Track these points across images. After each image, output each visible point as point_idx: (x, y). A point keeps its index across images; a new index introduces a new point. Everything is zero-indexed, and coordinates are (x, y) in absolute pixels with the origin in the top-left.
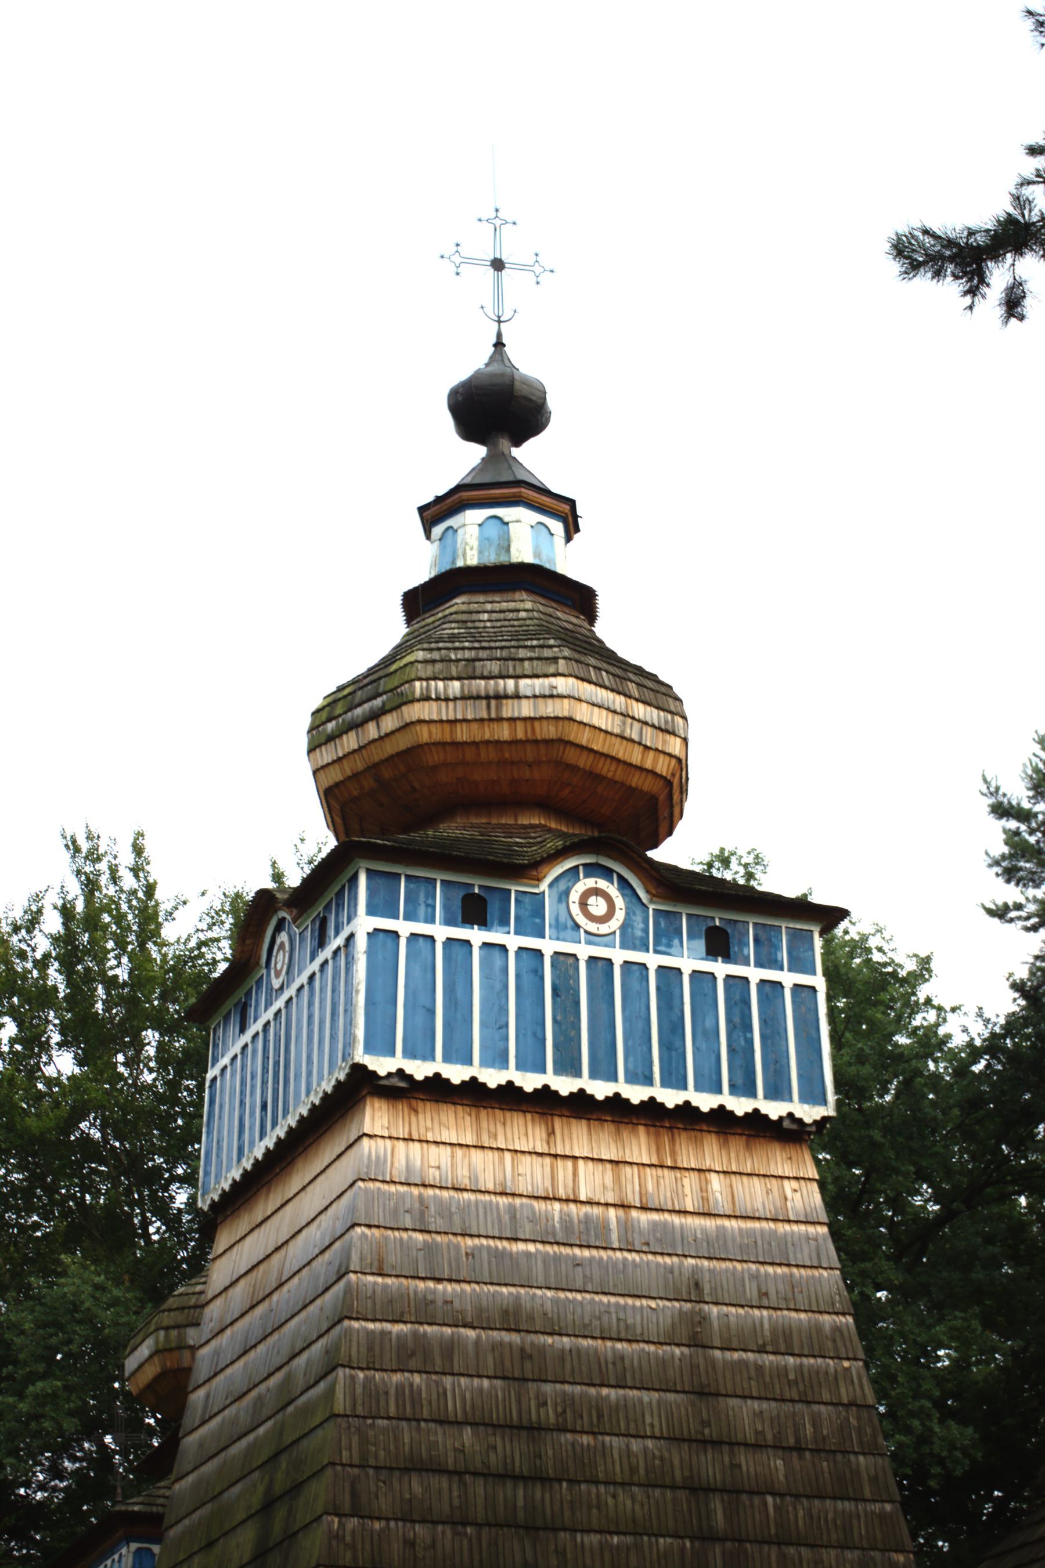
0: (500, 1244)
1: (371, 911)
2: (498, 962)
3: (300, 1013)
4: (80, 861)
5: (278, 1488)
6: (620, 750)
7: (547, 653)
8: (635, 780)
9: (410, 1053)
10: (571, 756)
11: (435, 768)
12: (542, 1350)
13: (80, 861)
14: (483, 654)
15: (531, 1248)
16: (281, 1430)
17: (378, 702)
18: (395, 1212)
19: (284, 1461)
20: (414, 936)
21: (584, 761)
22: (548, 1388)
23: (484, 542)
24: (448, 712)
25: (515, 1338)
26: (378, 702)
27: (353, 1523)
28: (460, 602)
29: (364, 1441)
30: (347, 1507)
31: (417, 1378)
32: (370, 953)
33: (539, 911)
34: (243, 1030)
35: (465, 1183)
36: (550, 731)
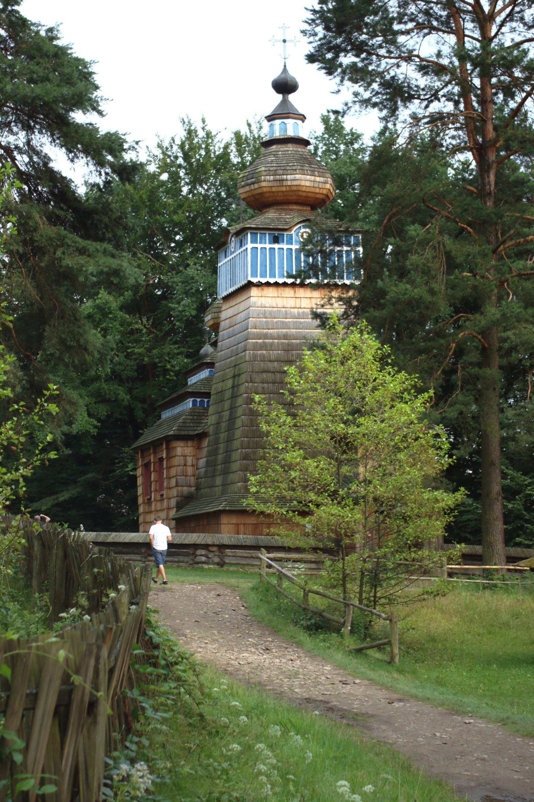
0: (283, 320)
1: (252, 242)
2: (282, 252)
3: (237, 259)
4: (185, 126)
5: (236, 374)
6: (313, 190)
7: (294, 168)
8: (318, 196)
9: (261, 276)
10: (301, 193)
11: (268, 197)
12: (293, 343)
13: (185, 126)
14: (279, 168)
15: (290, 320)
16: (236, 360)
17: (253, 180)
18: (258, 314)
19: (237, 367)
20: (262, 248)
21: (304, 194)
22: (294, 352)
23: (281, 129)
24: (270, 184)
25: (286, 341)
26: (253, 180)
27: (251, 384)
28: (274, 147)
29: (253, 367)
30: (249, 380)
31: (264, 352)
32: (252, 253)
33: (291, 238)
34: (226, 257)
35: (275, 306)
36: (295, 188)
